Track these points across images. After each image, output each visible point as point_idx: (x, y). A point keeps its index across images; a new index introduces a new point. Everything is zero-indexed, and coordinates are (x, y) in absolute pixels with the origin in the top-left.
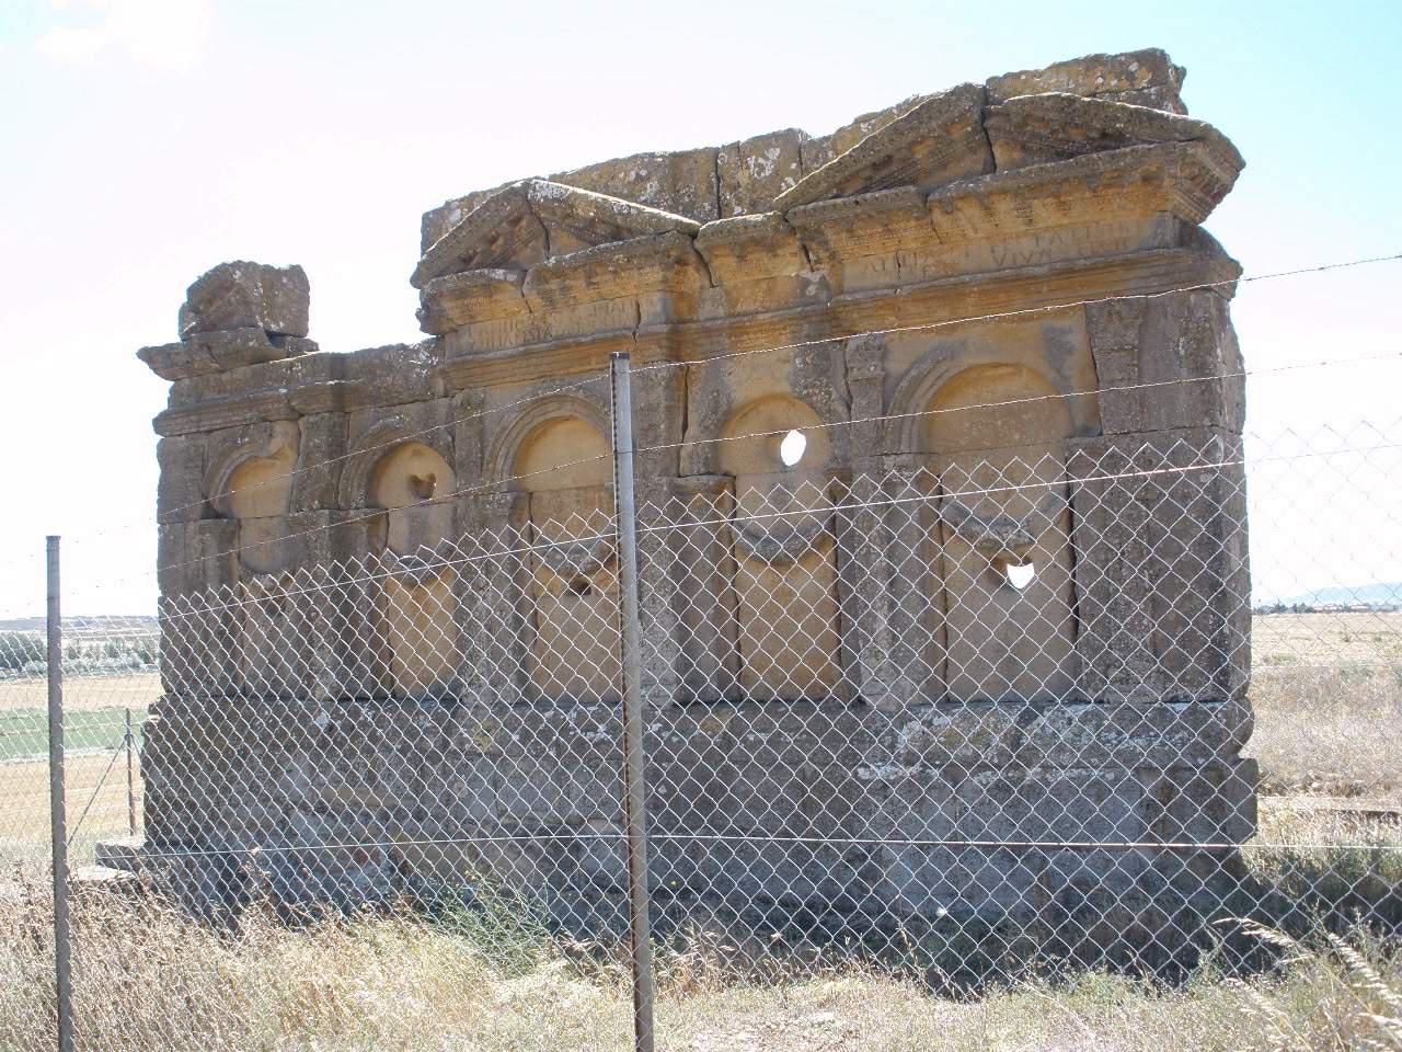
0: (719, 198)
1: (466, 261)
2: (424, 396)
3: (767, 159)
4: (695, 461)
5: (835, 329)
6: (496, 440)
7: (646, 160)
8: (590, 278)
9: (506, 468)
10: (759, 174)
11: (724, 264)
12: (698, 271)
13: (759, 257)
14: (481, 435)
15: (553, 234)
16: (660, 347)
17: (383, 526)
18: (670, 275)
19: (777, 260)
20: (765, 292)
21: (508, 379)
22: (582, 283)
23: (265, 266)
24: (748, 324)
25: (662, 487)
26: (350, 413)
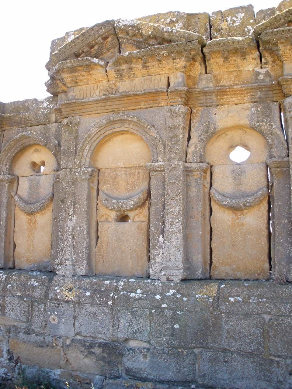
0: (211, 34)
1: (77, 55)
2: (44, 122)
3: (237, 18)
4: (195, 154)
5: (275, 95)
6: (85, 141)
7: (176, 14)
8: (145, 63)
9: (89, 155)
10: (233, 24)
11: (215, 62)
12: (201, 65)
13: (236, 59)
14: (76, 138)
15: (123, 46)
16: (181, 98)
17: (15, 185)
18: (188, 64)
19: (245, 61)
20: (236, 77)
21: (93, 112)
22: (140, 66)
24: (228, 90)
25: (180, 166)
26: (5, 130)
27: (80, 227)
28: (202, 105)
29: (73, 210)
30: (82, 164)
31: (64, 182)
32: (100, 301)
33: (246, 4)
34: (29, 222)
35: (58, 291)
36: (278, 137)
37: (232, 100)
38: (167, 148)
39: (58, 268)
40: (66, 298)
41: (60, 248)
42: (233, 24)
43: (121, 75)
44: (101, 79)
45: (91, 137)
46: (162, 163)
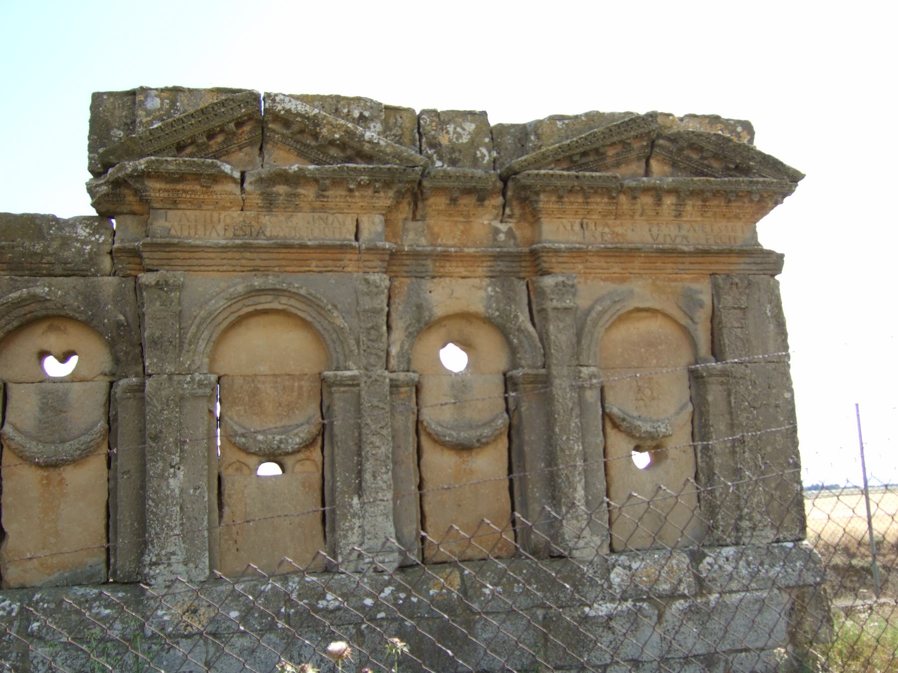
1: (180, 148)
10: (457, 139)
12: (409, 204)
19: (480, 209)
23: (587, 115)
27: (195, 489)
28: (409, 275)
29: (180, 456)
30: (194, 367)
31: (157, 400)
32: (261, 624)
33: (478, 109)
34: (45, 482)
35: (166, 618)
36: (529, 336)
37: (458, 270)
38: (362, 348)
39: (152, 573)
40: (185, 630)
41: (153, 532)
42: (457, 139)
43: (271, 204)
44: (229, 204)
45: (213, 316)
46: (355, 372)
